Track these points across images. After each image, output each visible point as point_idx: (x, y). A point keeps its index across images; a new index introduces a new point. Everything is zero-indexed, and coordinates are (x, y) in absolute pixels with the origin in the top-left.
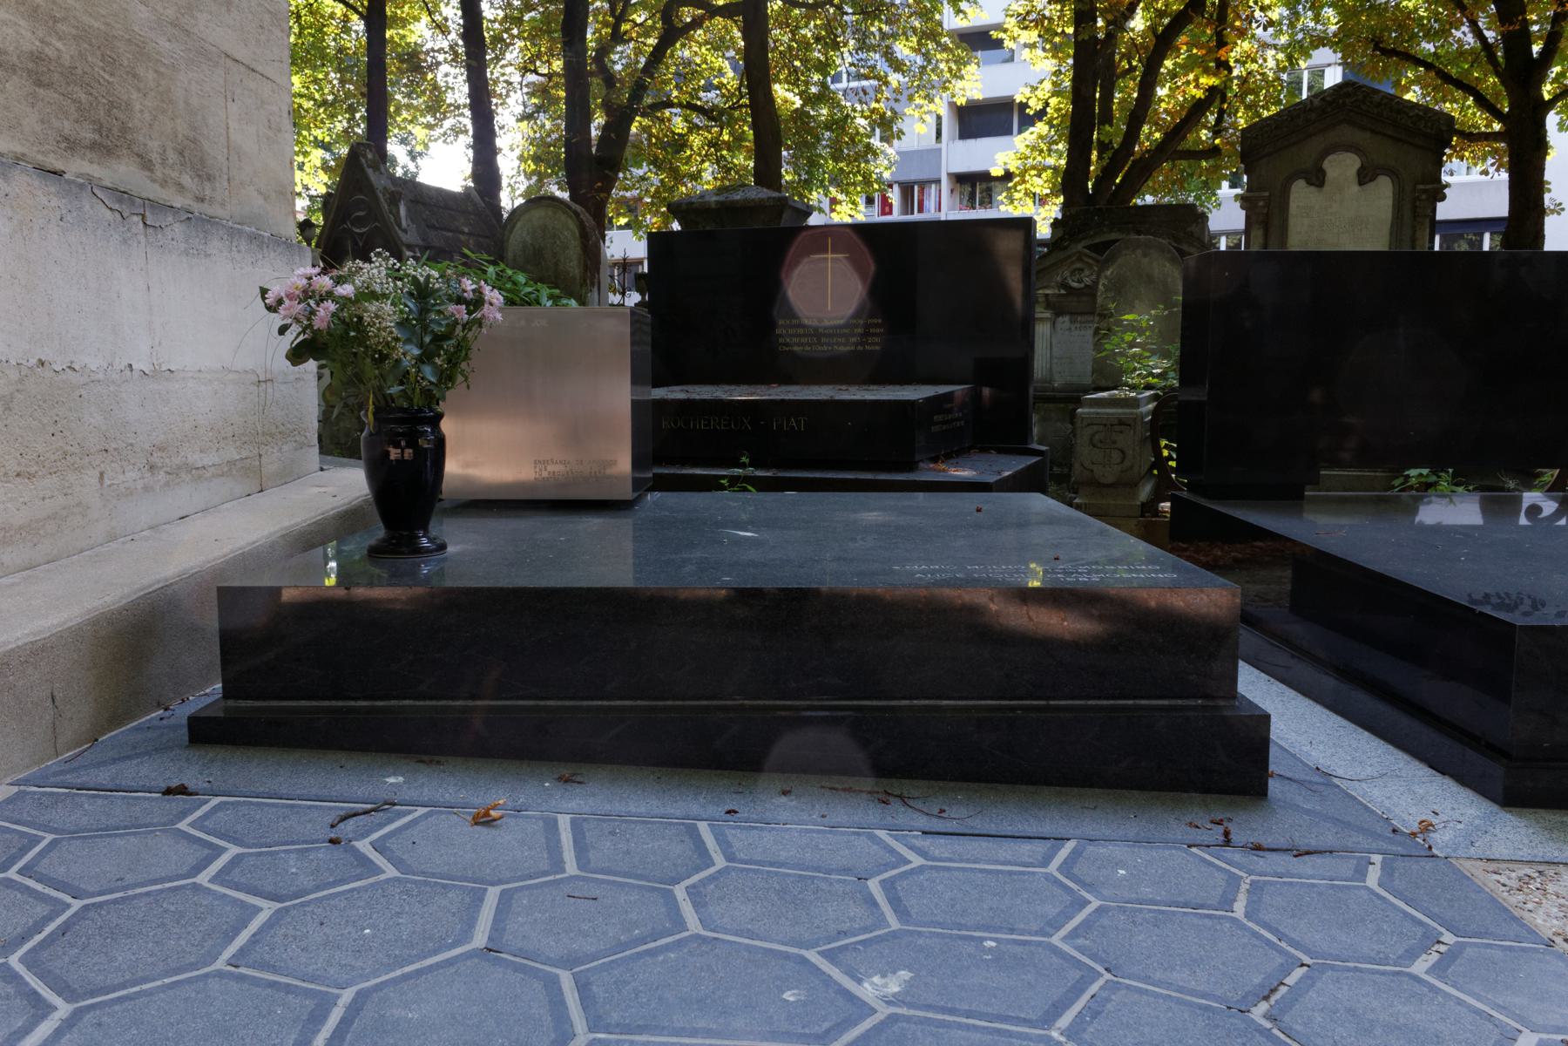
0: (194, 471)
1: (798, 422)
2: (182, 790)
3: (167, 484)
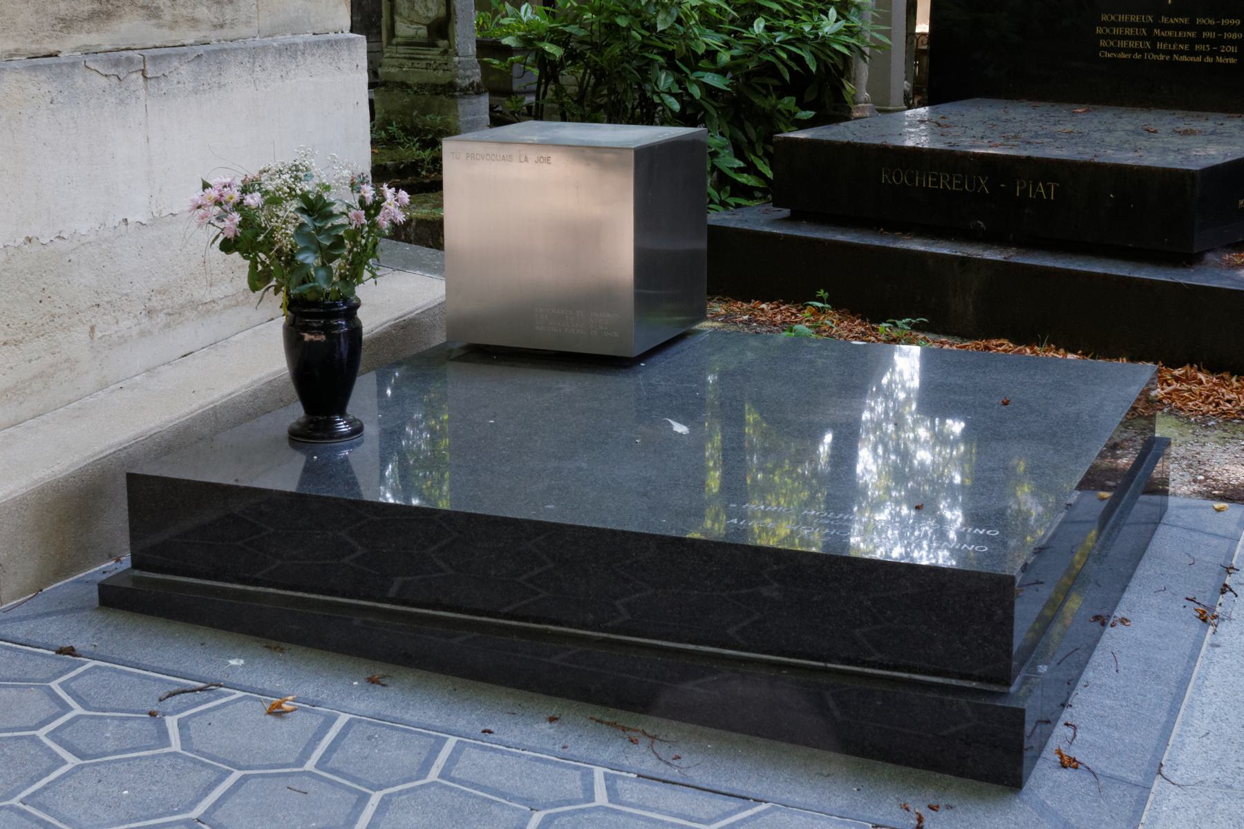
0: (201, 307)
1: (1047, 189)
2: (71, 651)
3: (168, 326)
